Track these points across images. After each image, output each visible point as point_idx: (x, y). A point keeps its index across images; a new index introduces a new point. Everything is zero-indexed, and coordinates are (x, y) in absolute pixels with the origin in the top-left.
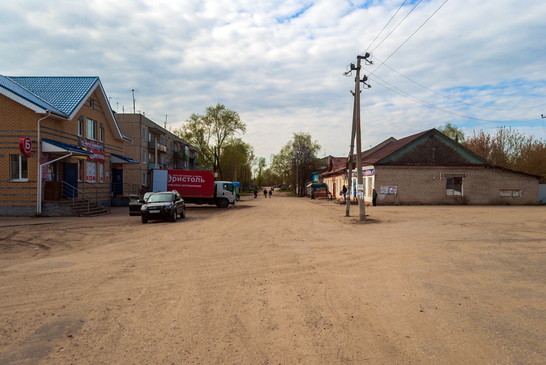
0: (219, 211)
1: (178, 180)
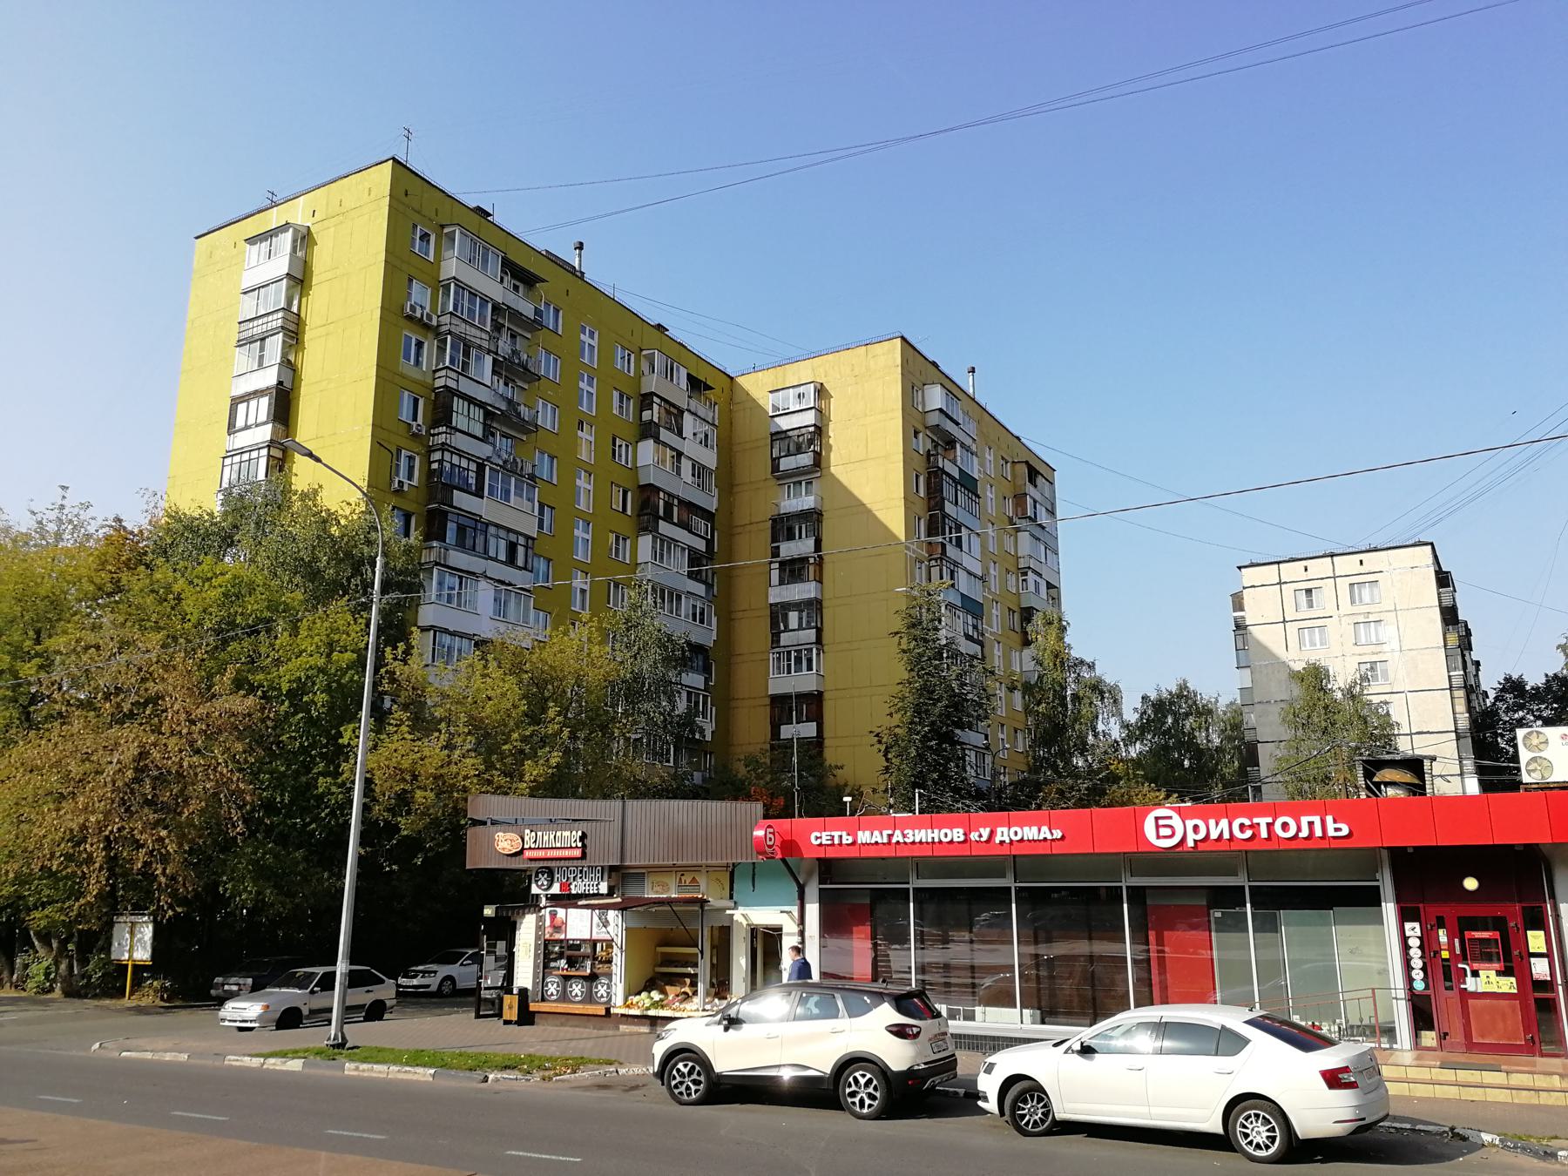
0: (438, 1011)
1: (1224, 823)
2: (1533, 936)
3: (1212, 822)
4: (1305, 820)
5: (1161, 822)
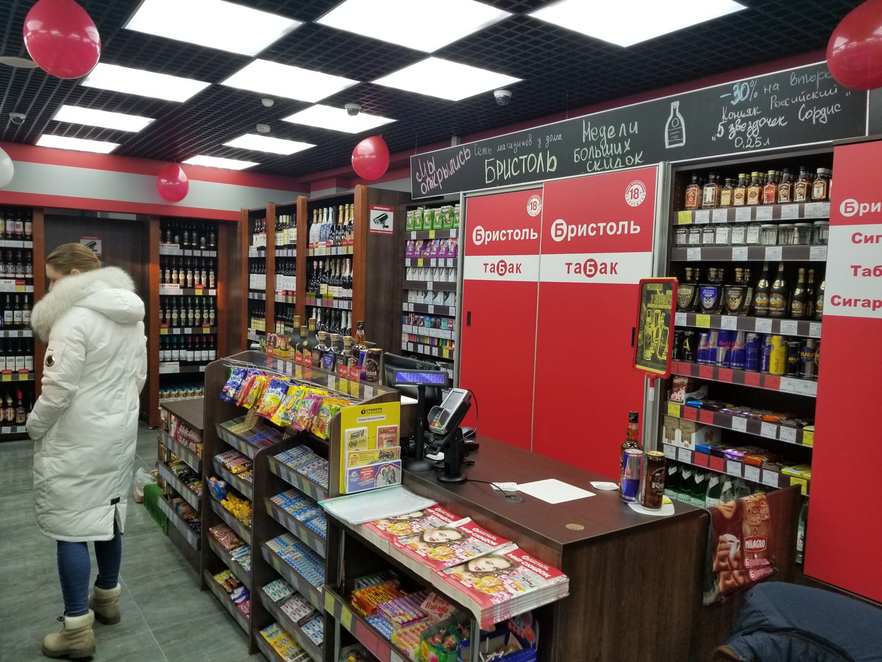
2: (270, 636)
3: (873, 204)
4: (621, 223)
5: (848, 205)
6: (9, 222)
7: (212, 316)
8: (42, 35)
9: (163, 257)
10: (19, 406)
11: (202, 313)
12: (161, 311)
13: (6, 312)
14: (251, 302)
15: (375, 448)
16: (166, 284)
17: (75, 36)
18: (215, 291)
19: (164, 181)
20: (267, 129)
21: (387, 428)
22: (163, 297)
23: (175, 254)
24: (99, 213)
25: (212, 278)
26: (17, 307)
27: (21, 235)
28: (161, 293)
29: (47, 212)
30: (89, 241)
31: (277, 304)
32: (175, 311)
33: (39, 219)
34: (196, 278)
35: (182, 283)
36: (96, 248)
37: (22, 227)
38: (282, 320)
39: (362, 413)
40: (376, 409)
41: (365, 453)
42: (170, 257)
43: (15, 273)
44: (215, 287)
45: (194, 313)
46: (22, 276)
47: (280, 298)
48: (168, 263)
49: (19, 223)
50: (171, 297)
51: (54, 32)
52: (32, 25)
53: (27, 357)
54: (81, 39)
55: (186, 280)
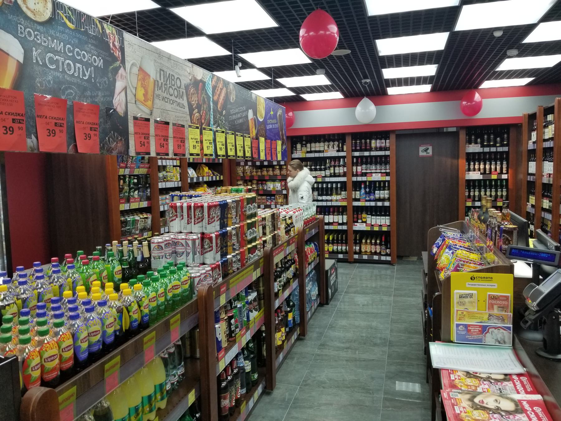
6: (378, 141)
7: (505, 193)
8: (306, 36)
9: (468, 154)
10: (383, 245)
11: (496, 191)
12: (467, 190)
13: (376, 192)
14: (529, 182)
15: (486, 311)
16: (470, 172)
17: (322, 32)
18: (506, 175)
19: (464, 103)
20: (515, 52)
21: (497, 295)
22: (469, 181)
23: (477, 151)
24: (445, 129)
25: (505, 166)
26: (382, 189)
27: (384, 148)
28: (467, 178)
29: (397, 133)
30: (424, 148)
31: (544, 184)
32: (477, 190)
33: (393, 137)
34: (493, 167)
35: (482, 171)
36: (428, 151)
37: (384, 143)
38: (547, 197)
39: (471, 279)
40: (487, 278)
41: (473, 313)
42: (474, 154)
43: (381, 170)
44: (507, 173)
45: (491, 191)
46: (385, 171)
47: (545, 180)
48: (472, 158)
49: (383, 141)
50: (474, 181)
51: (311, 33)
52: (302, 32)
53: (387, 217)
54: (325, 33)
55: (485, 169)
